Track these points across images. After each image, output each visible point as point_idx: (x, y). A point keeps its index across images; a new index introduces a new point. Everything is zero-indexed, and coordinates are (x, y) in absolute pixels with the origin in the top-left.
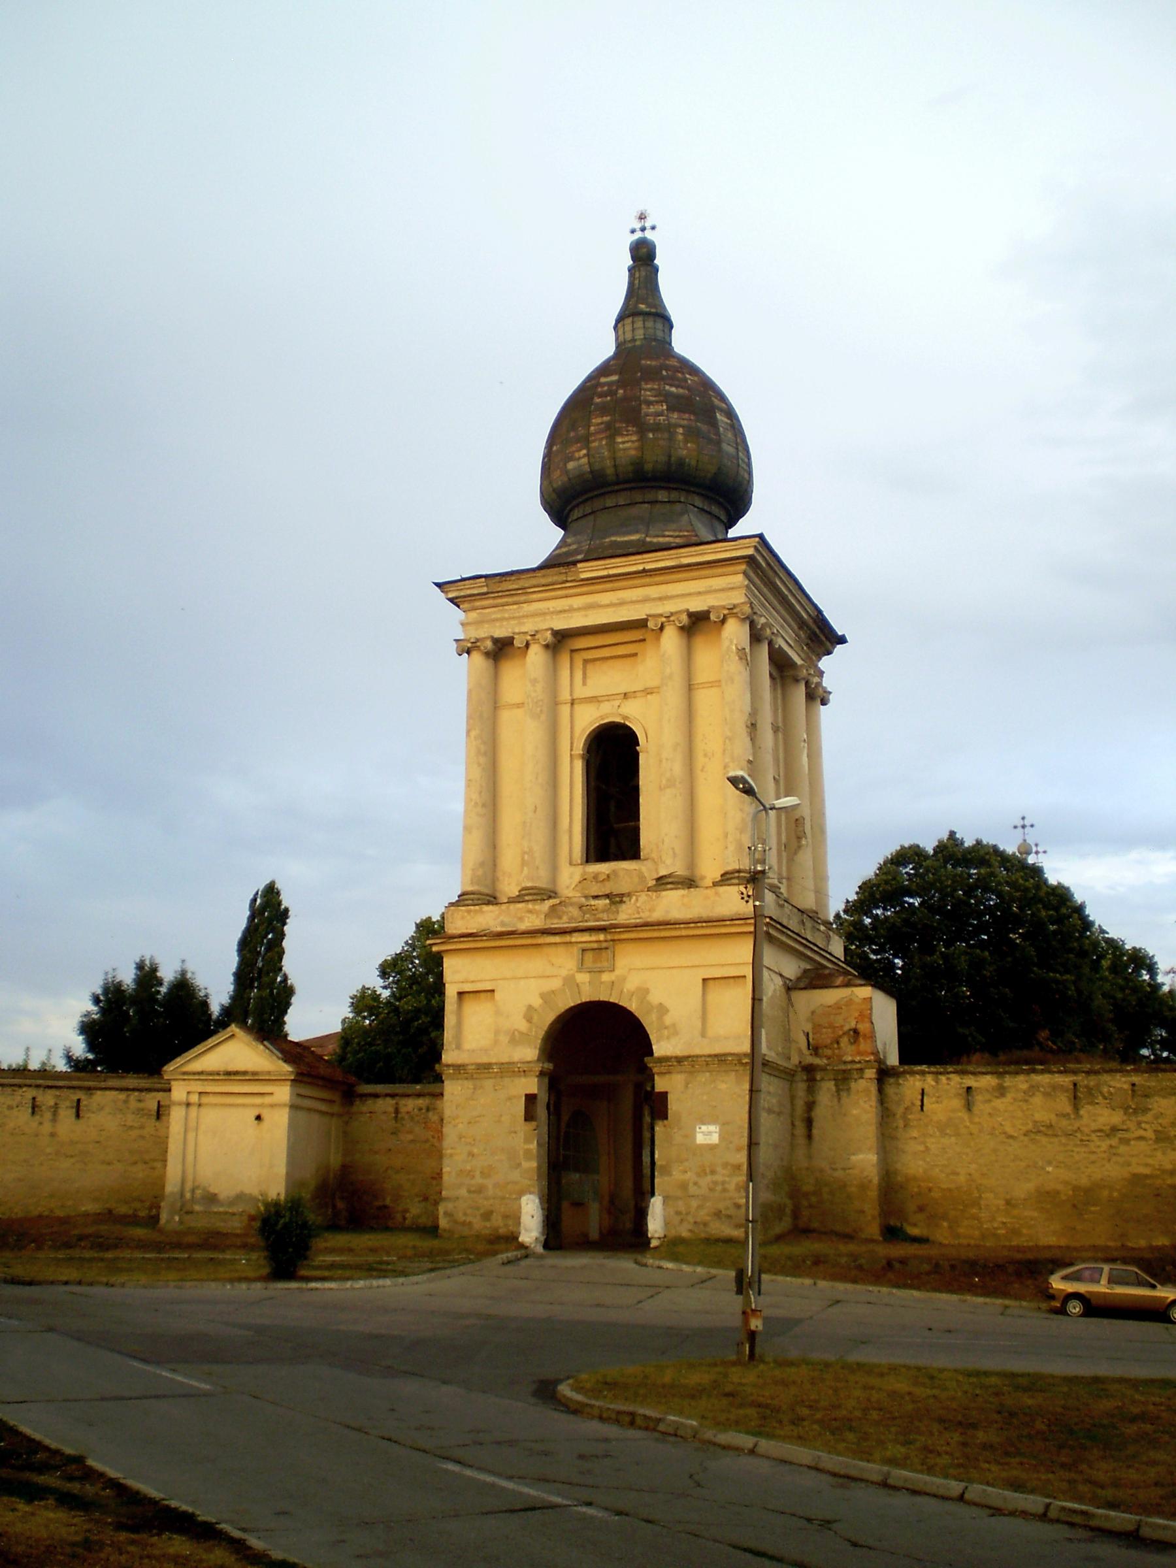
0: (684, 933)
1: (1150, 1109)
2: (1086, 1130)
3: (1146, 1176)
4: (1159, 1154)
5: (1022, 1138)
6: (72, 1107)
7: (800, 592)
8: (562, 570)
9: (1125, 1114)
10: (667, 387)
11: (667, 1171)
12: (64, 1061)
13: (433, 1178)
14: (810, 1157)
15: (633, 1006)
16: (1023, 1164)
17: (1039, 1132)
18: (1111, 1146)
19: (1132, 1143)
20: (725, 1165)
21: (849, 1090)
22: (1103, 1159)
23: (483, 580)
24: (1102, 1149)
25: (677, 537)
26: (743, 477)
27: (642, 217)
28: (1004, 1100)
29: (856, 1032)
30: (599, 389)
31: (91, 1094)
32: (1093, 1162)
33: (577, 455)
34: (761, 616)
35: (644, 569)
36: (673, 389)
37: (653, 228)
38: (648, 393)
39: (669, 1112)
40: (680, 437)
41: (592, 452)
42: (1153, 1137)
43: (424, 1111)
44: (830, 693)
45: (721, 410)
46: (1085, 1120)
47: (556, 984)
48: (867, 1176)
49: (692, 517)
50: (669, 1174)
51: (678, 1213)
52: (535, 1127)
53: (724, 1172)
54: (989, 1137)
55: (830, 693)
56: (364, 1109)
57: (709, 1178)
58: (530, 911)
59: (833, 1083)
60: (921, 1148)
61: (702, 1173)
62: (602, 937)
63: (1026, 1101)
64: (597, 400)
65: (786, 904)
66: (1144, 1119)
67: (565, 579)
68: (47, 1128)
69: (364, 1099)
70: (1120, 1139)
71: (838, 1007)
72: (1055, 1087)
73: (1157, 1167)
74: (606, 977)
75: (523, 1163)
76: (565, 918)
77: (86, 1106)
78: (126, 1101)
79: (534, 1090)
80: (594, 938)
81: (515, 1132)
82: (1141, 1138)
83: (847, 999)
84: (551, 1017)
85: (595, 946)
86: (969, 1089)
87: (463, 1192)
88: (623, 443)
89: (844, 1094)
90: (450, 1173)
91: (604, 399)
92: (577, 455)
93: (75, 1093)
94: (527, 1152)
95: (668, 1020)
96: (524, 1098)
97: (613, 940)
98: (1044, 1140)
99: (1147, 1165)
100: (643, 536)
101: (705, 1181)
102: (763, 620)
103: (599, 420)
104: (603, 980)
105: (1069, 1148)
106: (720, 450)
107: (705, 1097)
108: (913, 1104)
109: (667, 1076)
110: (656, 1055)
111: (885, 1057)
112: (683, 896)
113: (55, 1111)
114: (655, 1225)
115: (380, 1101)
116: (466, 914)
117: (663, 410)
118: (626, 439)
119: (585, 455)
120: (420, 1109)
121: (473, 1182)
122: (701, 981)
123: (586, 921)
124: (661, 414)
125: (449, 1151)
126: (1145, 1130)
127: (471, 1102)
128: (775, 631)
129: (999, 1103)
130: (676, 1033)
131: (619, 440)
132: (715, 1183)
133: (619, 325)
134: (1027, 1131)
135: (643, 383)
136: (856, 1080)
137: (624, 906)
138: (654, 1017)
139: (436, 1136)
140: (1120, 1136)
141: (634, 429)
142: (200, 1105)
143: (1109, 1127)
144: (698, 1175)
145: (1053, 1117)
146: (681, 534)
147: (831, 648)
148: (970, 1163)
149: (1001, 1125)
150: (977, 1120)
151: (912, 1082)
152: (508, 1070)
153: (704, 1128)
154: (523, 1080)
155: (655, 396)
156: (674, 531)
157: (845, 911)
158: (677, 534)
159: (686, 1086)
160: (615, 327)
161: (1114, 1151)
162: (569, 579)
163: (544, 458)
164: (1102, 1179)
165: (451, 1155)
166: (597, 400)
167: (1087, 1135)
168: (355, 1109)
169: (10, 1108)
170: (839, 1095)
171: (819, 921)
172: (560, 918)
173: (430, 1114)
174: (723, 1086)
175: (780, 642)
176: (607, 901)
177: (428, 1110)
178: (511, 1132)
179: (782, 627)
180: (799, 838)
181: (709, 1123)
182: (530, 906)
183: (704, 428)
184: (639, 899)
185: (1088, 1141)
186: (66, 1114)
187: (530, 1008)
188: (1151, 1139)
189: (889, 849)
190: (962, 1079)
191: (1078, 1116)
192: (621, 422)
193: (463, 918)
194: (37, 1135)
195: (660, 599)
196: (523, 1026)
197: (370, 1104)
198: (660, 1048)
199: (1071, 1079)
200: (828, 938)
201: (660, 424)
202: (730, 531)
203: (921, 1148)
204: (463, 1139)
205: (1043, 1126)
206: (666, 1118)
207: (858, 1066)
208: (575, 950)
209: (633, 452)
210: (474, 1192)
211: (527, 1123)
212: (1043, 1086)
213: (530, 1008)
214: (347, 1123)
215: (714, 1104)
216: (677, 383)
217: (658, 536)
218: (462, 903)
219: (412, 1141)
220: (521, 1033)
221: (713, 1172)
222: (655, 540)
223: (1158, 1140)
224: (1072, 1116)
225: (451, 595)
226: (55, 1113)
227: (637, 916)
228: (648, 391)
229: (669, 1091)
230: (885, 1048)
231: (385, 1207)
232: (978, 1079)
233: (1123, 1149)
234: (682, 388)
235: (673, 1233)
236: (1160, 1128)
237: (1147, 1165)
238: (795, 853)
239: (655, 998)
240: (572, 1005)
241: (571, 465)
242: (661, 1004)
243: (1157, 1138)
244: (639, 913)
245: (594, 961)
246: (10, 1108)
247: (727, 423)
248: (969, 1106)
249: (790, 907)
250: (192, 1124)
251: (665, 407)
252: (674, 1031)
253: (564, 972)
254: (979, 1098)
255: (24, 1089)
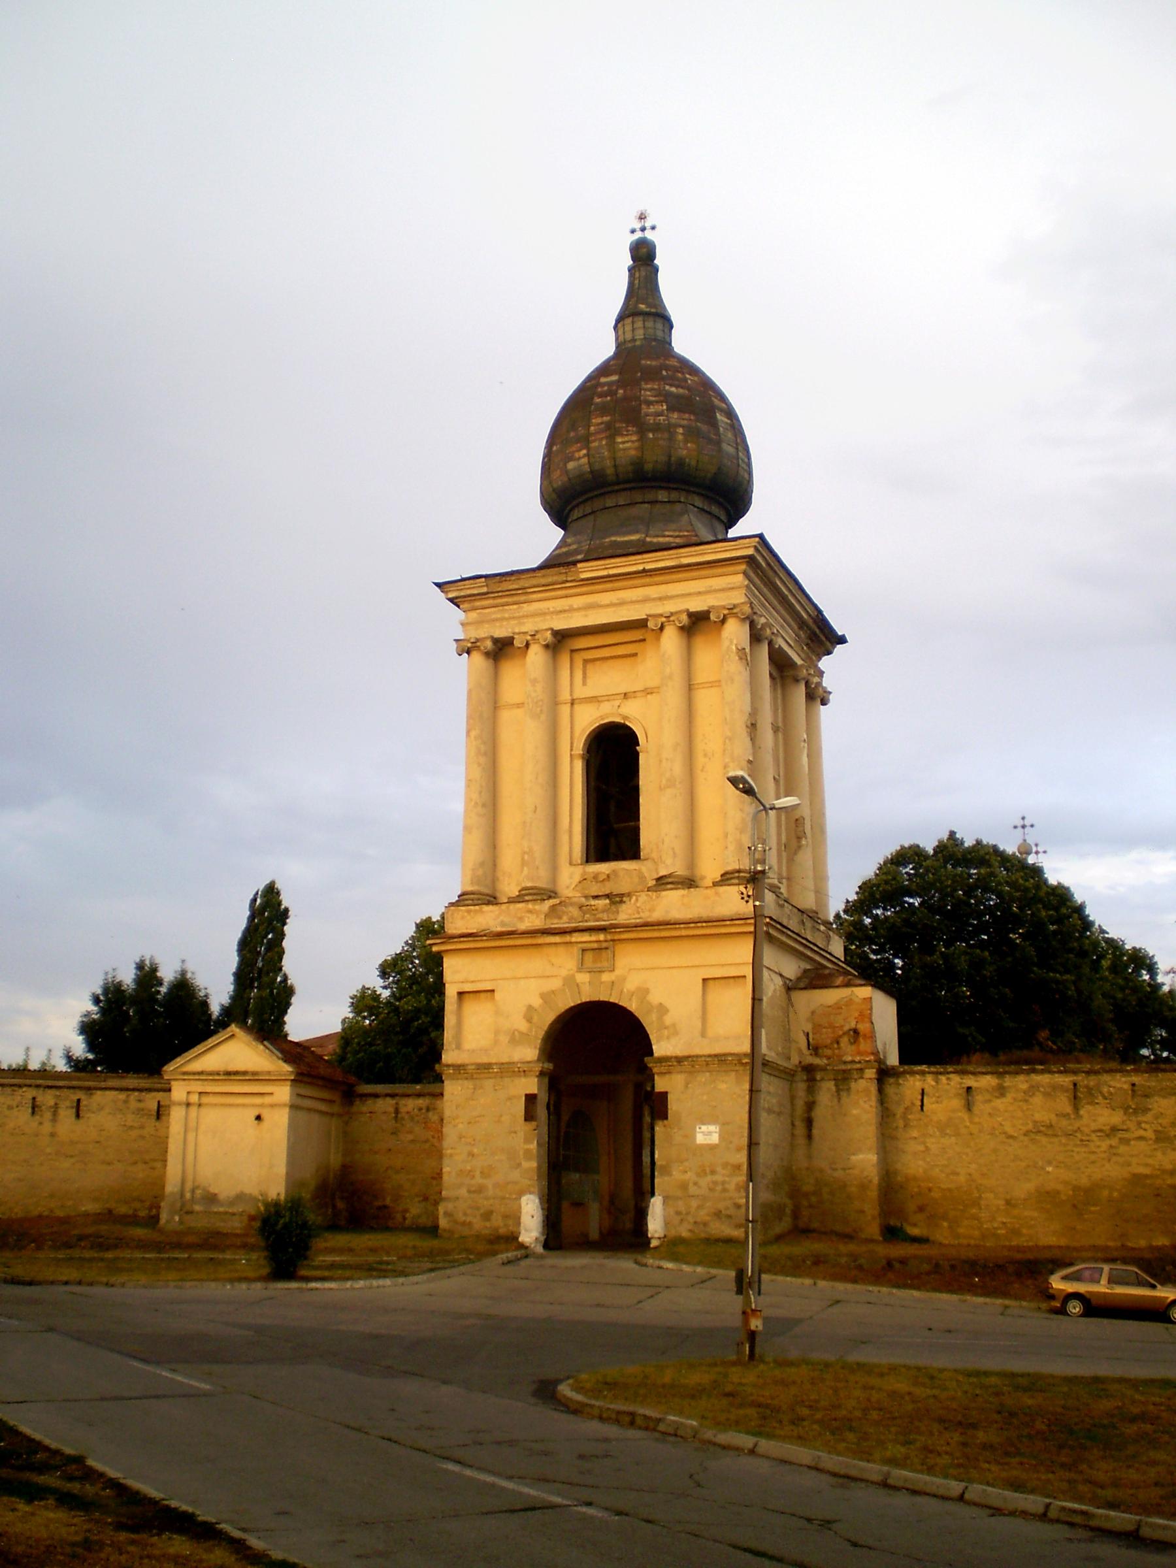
0: (684, 933)
1: (1150, 1109)
2: (1086, 1130)
3: (1147, 1176)
4: (1159, 1154)
5: (1022, 1138)
6: (72, 1107)
7: (800, 593)
8: (562, 570)
9: (1125, 1114)
10: (667, 387)
11: (666, 1171)
12: (64, 1061)
13: (433, 1178)
14: (810, 1157)
15: (633, 1006)
16: (1023, 1164)
17: (1040, 1132)
18: (1111, 1146)
19: (1132, 1142)
20: (725, 1165)
21: (848, 1090)
22: (1103, 1159)
23: (483, 580)
24: (1102, 1149)
25: (677, 537)
26: (743, 477)
27: (642, 217)
28: (1004, 1100)
29: (856, 1032)
30: (599, 390)
31: (91, 1094)
32: (1093, 1162)
33: (577, 455)
34: (761, 616)
35: (644, 569)
36: (673, 389)
37: (653, 228)
38: (648, 393)
39: (669, 1112)
40: (680, 437)
41: (592, 452)
42: (1153, 1137)
43: (424, 1111)
44: (830, 693)
45: (721, 410)
46: (1085, 1121)
47: (556, 984)
48: (867, 1176)
49: (692, 517)
50: (669, 1174)
51: (678, 1213)
52: (535, 1127)
53: (724, 1172)
54: (989, 1137)
55: (830, 693)
56: (364, 1109)
57: (709, 1178)
58: (530, 911)
59: (833, 1083)
60: (921, 1148)
61: (702, 1172)
62: (602, 937)
63: (1026, 1101)
64: (598, 400)
65: (786, 904)
66: (1144, 1119)
67: (565, 579)
68: (47, 1127)
69: (364, 1099)
70: (1120, 1139)
71: (837, 1007)
72: (1055, 1087)
73: (1157, 1167)
74: (606, 977)
75: (523, 1163)
76: (565, 918)
77: (86, 1106)
78: (126, 1102)
79: (534, 1090)
80: (593, 938)
81: (515, 1132)
82: (1141, 1138)
83: (847, 999)
84: (551, 1017)
85: (595, 945)
86: (969, 1089)
87: (463, 1192)
88: (623, 443)
89: (843, 1094)
90: (450, 1173)
91: (604, 399)
92: (577, 455)
93: (75, 1093)
94: (527, 1151)
95: (668, 1020)
96: (524, 1098)
97: (613, 940)
98: (1044, 1140)
99: (1147, 1165)
100: (643, 536)
101: (705, 1182)
102: (763, 620)
103: (599, 420)
104: (603, 980)
105: (1069, 1148)
106: (720, 450)
107: (705, 1097)
108: (913, 1104)
109: (667, 1076)
110: (656, 1055)
111: (885, 1057)
112: (683, 896)
113: (55, 1111)
114: (655, 1225)
115: (380, 1102)
116: (466, 914)
117: (663, 411)
118: (626, 439)
119: (585, 456)
120: (420, 1109)
121: (473, 1182)
122: (701, 981)
123: (586, 921)
124: (661, 414)
125: (449, 1152)
126: (1145, 1130)
127: (471, 1102)
128: (775, 631)
129: (999, 1103)
130: (676, 1033)
131: (619, 440)
132: (715, 1183)
133: (619, 325)
134: (1027, 1131)
135: (643, 383)
136: (856, 1080)
137: (624, 907)
138: (654, 1017)
139: (436, 1136)
140: (1120, 1136)
141: (634, 429)
142: (200, 1105)
143: (1109, 1127)
144: (698, 1175)
145: (1053, 1116)
146: (681, 534)
147: (831, 648)
148: (970, 1163)
149: (1001, 1125)
150: (976, 1120)
151: (912, 1082)
152: (508, 1070)
153: (704, 1128)
154: (523, 1080)
155: (655, 396)
156: (674, 531)
157: (845, 911)
158: (677, 534)
159: (686, 1087)
160: (615, 327)
161: (1114, 1151)
162: (569, 579)
163: (544, 458)
164: (1102, 1179)
165: (451, 1155)
166: (598, 400)
167: (1087, 1135)
168: (354, 1109)
169: (10, 1108)
170: (839, 1095)
171: (819, 921)
172: (560, 918)
173: (430, 1114)
174: (722, 1086)
175: (780, 642)
176: (607, 901)
177: (428, 1110)
178: (511, 1132)
179: (782, 626)
180: (799, 838)
181: (709, 1123)
182: (530, 906)
183: (704, 428)
184: (639, 898)
185: (1088, 1141)
186: (66, 1114)
187: (530, 1008)
188: (1151, 1139)
189: (889, 849)
190: (962, 1079)
191: (1079, 1116)
192: (621, 421)
193: (463, 918)
194: (37, 1135)
195: (660, 599)
196: (523, 1026)
197: (370, 1104)
198: (660, 1048)
199: (1071, 1079)
200: (828, 938)
201: (660, 424)
202: (730, 531)
203: (921, 1148)
204: (463, 1139)
205: (1043, 1126)
206: (666, 1118)
207: (858, 1066)
208: (576, 950)
209: (633, 452)
210: (474, 1192)
211: (527, 1123)
212: (1043, 1086)
213: (530, 1008)
214: (347, 1123)
215: (714, 1104)
216: (677, 383)
217: (658, 536)
218: (462, 903)
219: (413, 1141)
220: (521, 1033)
221: (713, 1172)
222: (655, 540)
223: (1158, 1140)
224: (1072, 1116)
225: (451, 595)
226: (55, 1113)
227: (638, 916)
228: (648, 391)
229: (669, 1091)
230: (885, 1048)
231: (385, 1207)
232: (978, 1079)
233: (1122, 1149)
234: (682, 388)
235: (673, 1233)
236: (1160, 1128)
237: (1147, 1165)
238: (795, 853)
239: (655, 998)
240: (572, 1005)
241: (571, 465)
242: (661, 1004)
243: (1157, 1138)
244: (639, 913)
245: (595, 961)
246: (10, 1108)
247: (727, 423)
248: (969, 1107)
249: (790, 907)
250: (192, 1124)
251: (665, 407)
252: (674, 1031)
253: (564, 972)
254: (979, 1098)
255: (24, 1089)
